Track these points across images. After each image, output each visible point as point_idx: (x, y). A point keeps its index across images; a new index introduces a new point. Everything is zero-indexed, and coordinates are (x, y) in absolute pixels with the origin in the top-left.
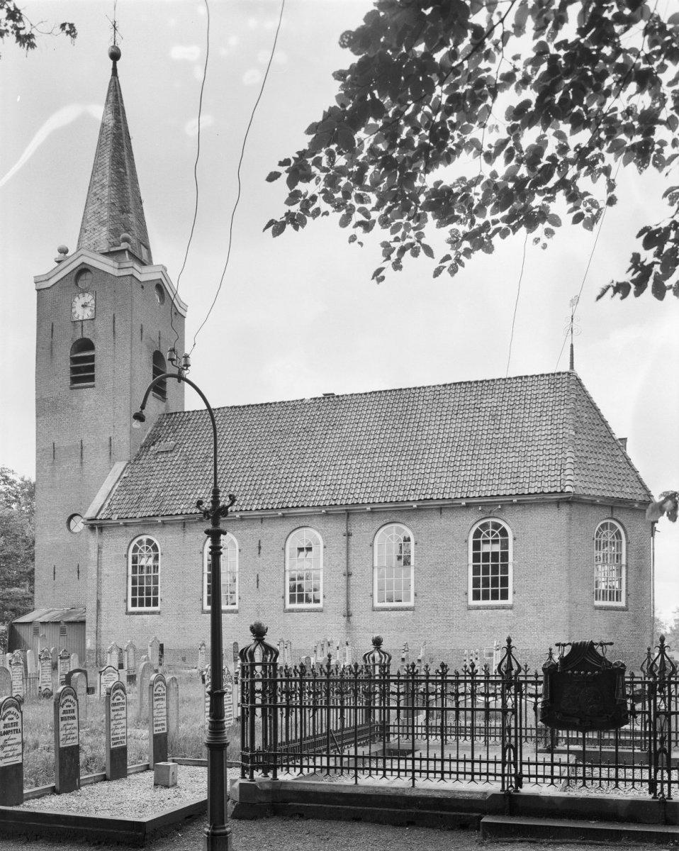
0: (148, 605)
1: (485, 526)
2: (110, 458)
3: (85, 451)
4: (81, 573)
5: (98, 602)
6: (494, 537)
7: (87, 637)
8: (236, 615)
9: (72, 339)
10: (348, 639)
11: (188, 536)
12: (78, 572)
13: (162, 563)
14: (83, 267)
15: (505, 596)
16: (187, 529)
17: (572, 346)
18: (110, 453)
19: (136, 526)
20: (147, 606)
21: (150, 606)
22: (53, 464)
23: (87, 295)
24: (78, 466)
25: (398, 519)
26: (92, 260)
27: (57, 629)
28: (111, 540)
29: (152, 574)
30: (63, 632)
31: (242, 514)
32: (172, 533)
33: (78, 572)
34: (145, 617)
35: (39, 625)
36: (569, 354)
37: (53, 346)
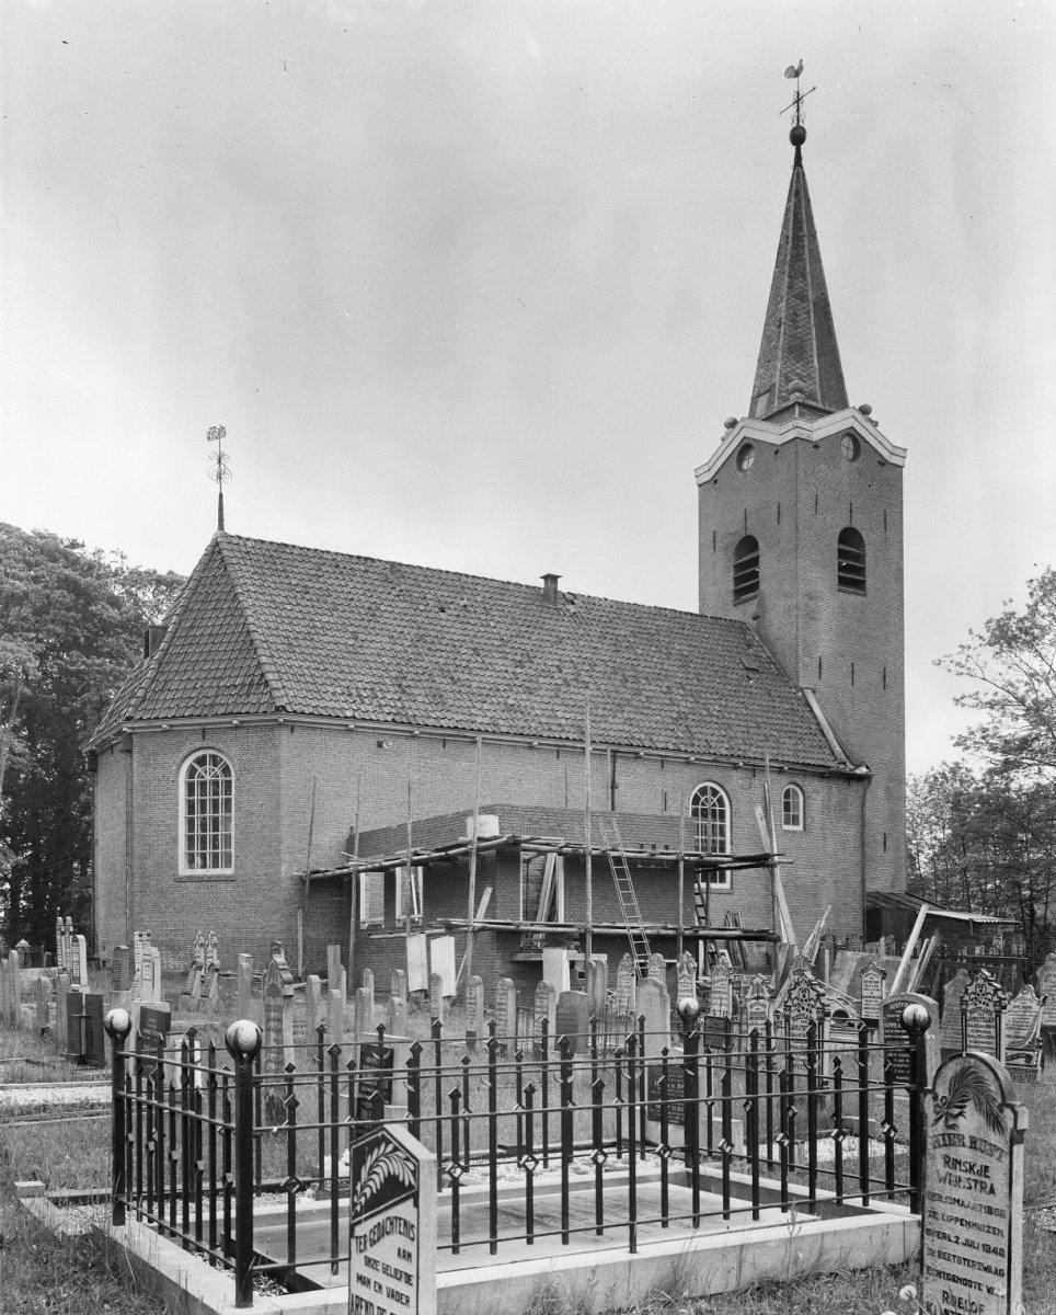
17: (221, 496)
36: (217, 506)
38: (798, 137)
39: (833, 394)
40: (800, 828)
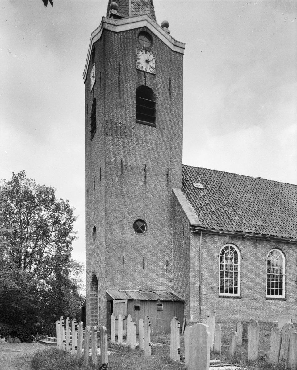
1: (227, 248)
2: (168, 183)
3: (148, 173)
4: (146, 265)
5: (200, 288)
6: (228, 254)
7: (191, 313)
8: (285, 302)
9: (137, 83)
10: (207, 317)
11: (258, 249)
12: (143, 264)
13: (218, 263)
14: (146, 30)
15: (236, 292)
16: (258, 244)
18: (168, 180)
19: (226, 236)
20: (272, 294)
21: (232, 293)
22: (121, 176)
23: (149, 53)
24: (142, 183)
25: (235, 243)
26: (154, 29)
27: (155, 307)
28: (208, 244)
29: (234, 271)
30: (160, 308)
31: (223, 232)
32: (248, 245)
33: (143, 264)
34: (232, 300)
35: (139, 302)
37: (121, 82)
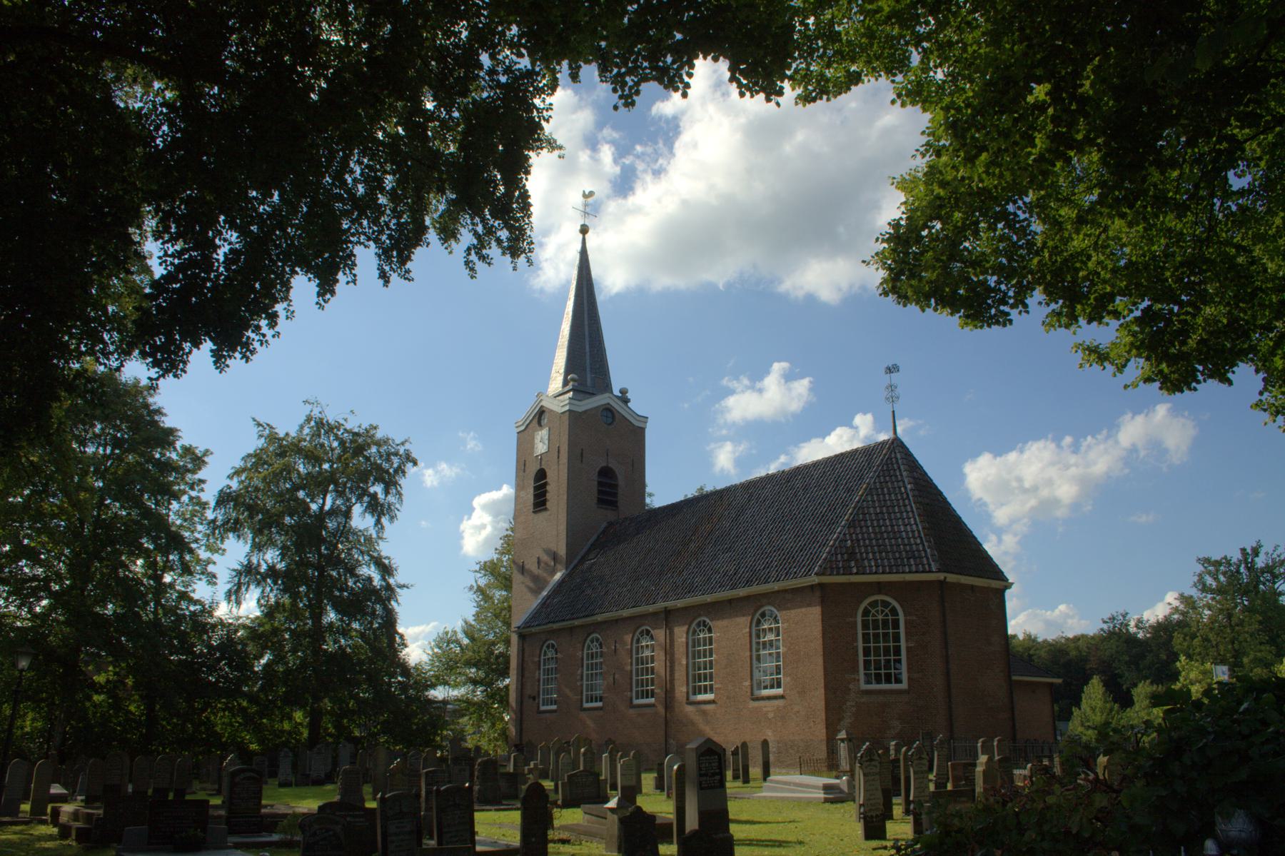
0: (888, 681)
38: (584, 230)
39: (607, 387)
40: (864, 686)
